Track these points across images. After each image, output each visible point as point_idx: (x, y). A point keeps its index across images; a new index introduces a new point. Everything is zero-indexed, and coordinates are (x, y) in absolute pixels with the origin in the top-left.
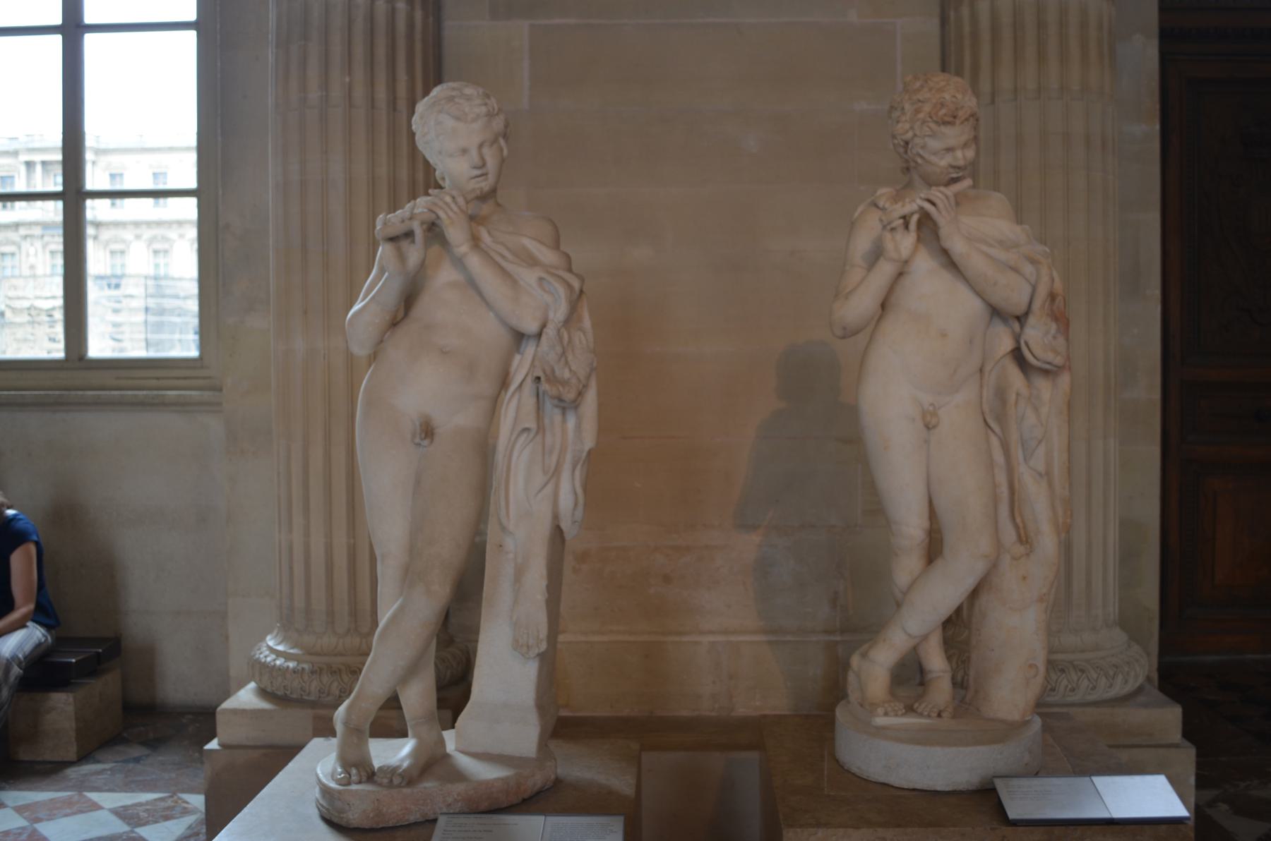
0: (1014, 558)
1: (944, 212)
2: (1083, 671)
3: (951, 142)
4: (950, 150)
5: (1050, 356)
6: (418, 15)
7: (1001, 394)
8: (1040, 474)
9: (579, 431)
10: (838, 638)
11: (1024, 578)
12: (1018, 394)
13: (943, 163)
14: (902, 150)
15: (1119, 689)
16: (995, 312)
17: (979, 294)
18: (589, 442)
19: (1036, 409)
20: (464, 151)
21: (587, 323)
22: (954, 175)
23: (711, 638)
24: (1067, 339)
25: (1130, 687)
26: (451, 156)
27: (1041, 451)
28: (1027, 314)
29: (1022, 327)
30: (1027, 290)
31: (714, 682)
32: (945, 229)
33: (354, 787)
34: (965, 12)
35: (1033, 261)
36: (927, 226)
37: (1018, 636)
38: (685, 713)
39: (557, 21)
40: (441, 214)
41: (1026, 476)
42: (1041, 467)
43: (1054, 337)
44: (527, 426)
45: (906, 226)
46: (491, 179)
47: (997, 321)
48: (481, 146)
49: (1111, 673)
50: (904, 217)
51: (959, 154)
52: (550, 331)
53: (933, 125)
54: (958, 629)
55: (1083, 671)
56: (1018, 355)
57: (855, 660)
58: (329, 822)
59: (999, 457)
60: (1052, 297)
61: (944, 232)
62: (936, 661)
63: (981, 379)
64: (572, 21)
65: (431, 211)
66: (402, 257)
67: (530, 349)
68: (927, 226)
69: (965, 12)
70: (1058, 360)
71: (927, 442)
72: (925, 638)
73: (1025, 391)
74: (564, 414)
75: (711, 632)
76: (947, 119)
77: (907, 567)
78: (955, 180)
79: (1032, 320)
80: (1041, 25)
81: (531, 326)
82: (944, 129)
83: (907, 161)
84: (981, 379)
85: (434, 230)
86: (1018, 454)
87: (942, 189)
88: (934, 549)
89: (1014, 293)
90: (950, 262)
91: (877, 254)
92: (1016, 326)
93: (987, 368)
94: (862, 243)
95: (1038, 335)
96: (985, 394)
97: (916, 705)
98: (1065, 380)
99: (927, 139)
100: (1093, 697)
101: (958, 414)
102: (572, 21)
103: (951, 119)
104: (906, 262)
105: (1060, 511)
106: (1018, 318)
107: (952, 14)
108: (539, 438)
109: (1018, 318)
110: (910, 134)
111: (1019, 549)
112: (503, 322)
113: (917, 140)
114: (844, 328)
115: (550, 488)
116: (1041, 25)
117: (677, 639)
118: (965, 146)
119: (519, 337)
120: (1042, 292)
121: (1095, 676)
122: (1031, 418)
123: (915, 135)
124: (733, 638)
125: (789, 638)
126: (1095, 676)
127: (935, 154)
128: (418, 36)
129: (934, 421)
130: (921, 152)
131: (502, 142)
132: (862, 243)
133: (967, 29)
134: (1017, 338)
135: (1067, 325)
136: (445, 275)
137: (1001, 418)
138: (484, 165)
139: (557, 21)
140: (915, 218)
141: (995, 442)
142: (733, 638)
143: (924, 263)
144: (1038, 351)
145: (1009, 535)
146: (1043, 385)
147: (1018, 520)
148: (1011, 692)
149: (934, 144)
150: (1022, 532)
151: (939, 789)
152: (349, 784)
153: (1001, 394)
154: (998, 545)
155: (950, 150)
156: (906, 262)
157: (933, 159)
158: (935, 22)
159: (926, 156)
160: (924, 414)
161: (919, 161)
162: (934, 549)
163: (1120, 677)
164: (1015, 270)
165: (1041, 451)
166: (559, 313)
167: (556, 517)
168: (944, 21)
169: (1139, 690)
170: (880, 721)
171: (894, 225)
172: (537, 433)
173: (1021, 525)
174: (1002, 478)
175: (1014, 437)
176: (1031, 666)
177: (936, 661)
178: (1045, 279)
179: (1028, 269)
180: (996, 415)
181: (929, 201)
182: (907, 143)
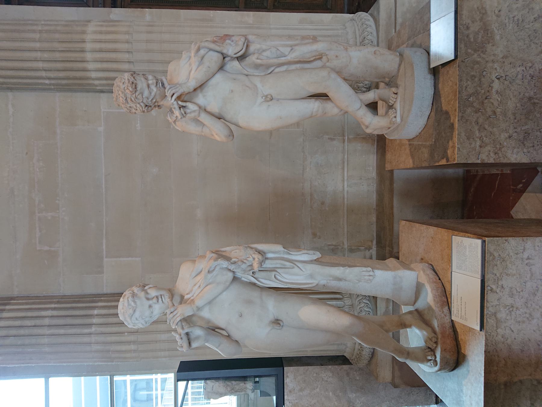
0: (328, 61)
1: (177, 90)
2: (364, 38)
3: (145, 85)
4: (148, 86)
5: (241, 43)
6: (100, 304)
7: (257, 66)
8: (292, 50)
9: (274, 250)
10: (346, 137)
11: (337, 56)
12: (257, 59)
13: (155, 89)
14: (150, 108)
15: (371, 22)
16: (221, 68)
17: (214, 75)
18: (279, 248)
19: (264, 51)
20: (150, 306)
21: (228, 249)
22: (161, 84)
23: (346, 186)
24: (233, 36)
25: (371, 19)
26: (152, 312)
27: (281, 49)
28: (222, 54)
29: (228, 56)
30: (211, 53)
31: (363, 185)
32: (184, 89)
33: (438, 359)
34: (97, 82)
35: (198, 50)
36: (183, 98)
37: (362, 58)
38: (375, 196)
39: (104, 247)
40: (178, 319)
41: (291, 57)
42: (289, 49)
43: (232, 41)
44: (273, 276)
45: (184, 107)
46: (162, 292)
47: (225, 68)
48: (148, 299)
49: (365, 26)
50: (180, 108)
51: (150, 82)
52: (232, 267)
53: (137, 94)
54: (358, 86)
55: (364, 38)
56: (241, 58)
57: (368, 131)
58: (452, 370)
59: (284, 68)
60: (214, 42)
61: (186, 90)
62: (371, 96)
63: (250, 75)
64: (104, 241)
65: (177, 324)
66: (197, 338)
67: (239, 274)
68: (183, 98)
69: (97, 82)
70: (243, 39)
71: (278, 100)
72: (361, 100)
73: (256, 56)
74: (267, 259)
75: (343, 186)
76: (134, 87)
77: (331, 109)
78: (163, 84)
79: (225, 51)
80: (101, 51)
81: (230, 275)
82: (139, 88)
83: (155, 106)
84: (250, 75)
85: (188, 320)
86: (283, 60)
87: (166, 91)
88: (322, 96)
89: (214, 59)
90: (200, 87)
91: (196, 121)
92: (227, 59)
93: (246, 72)
94: (192, 128)
95: (231, 50)
96: (257, 74)
97: (390, 104)
98: (250, 37)
99: (144, 97)
100: (375, 34)
101: (266, 86)
102: (104, 241)
103: (134, 85)
104: (200, 107)
105: (307, 41)
106: (224, 58)
107: (98, 88)
108: (278, 270)
109: (224, 58)
110: (142, 104)
111: (324, 59)
112: (227, 288)
113: (145, 101)
114: (229, 136)
115: (300, 265)
116: (101, 51)
117: (346, 200)
118: (147, 79)
119: (235, 279)
120: (212, 46)
121: (366, 33)
122: (267, 54)
123: (142, 102)
124: (346, 178)
125: (346, 156)
126: (366, 33)
127: (151, 93)
128: (109, 304)
129: (269, 97)
130: (150, 99)
131: (146, 288)
132: (192, 128)
133: (104, 82)
134: (233, 59)
135: (227, 35)
136: (206, 314)
137: (268, 66)
138: (157, 297)
139: (104, 247)
140: (180, 103)
141: (277, 70)
142: (346, 178)
143: (201, 99)
144: (239, 49)
145: (318, 63)
146: (252, 48)
147: (312, 59)
148: (387, 61)
149: (146, 93)
150: (317, 57)
151: (433, 93)
152: (435, 361)
153: (257, 66)
154: (323, 67)
155: (148, 86)
156: (200, 107)
157: (153, 94)
158: (102, 95)
159: (152, 97)
160: (266, 101)
161: (154, 100)
162: (322, 96)
163: (366, 22)
164: (203, 58)
165: (281, 49)
166: (225, 264)
167: (311, 262)
168: (102, 91)
169: (371, 15)
170: (398, 119)
171: (183, 113)
172: (276, 271)
173: (314, 58)
174: (293, 67)
175: (276, 61)
176: (375, 53)
177: (371, 96)
178: (207, 44)
179: (202, 52)
180: (267, 69)
181: (172, 96)
182: (146, 106)
